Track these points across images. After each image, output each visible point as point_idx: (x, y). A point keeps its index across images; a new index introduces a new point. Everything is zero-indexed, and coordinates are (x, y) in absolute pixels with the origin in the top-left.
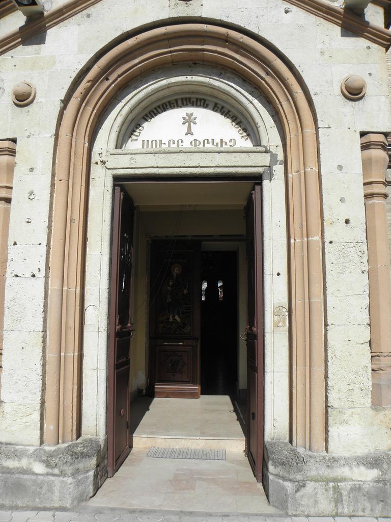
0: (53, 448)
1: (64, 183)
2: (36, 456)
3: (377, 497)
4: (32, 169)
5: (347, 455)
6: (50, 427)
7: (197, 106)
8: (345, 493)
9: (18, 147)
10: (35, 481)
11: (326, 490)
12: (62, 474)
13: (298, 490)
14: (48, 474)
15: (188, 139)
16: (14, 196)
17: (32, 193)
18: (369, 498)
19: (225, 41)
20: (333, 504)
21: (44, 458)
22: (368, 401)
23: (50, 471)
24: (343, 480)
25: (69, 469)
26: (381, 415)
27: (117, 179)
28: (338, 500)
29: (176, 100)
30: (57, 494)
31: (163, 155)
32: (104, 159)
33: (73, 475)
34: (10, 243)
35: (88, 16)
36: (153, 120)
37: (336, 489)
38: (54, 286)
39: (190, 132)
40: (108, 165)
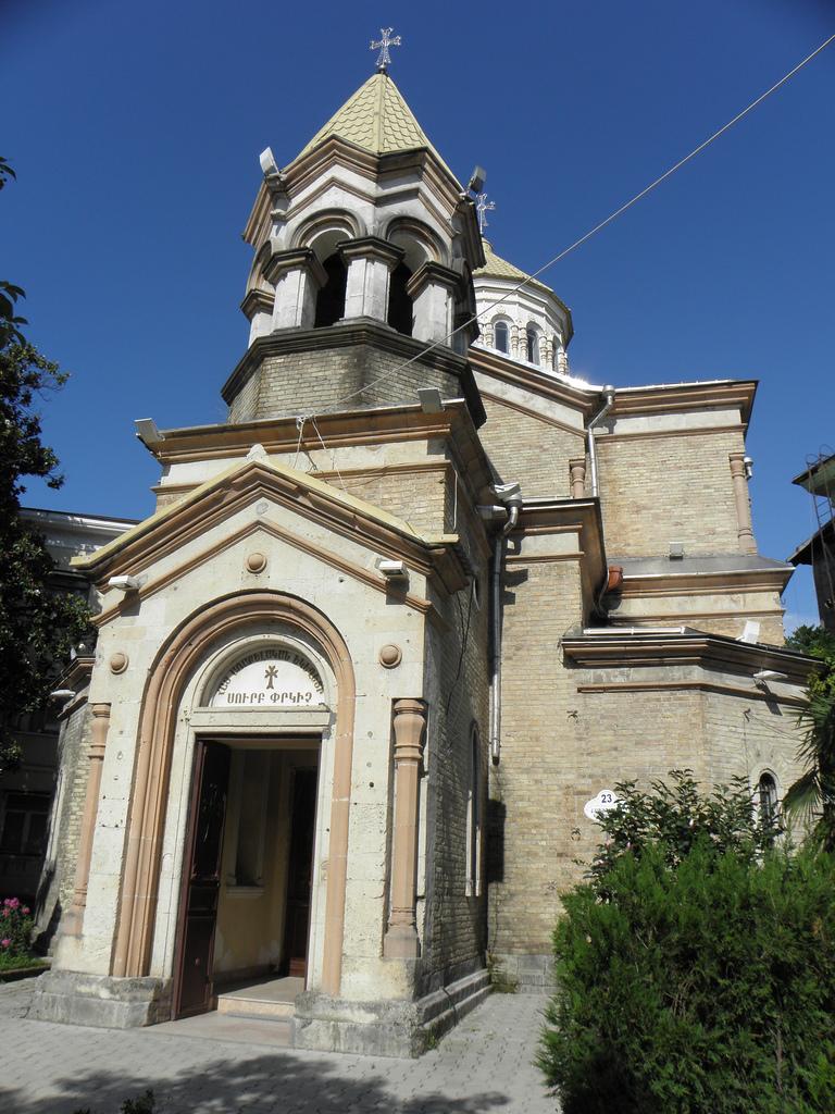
0: (119, 979)
1: (147, 744)
2: (104, 984)
3: (369, 1037)
4: (121, 732)
5: (353, 1000)
6: (119, 960)
7: (280, 658)
8: (342, 1032)
9: (113, 710)
10: (99, 1004)
11: (328, 1028)
12: (122, 999)
13: (304, 1026)
14: (111, 999)
15: (262, 698)
16: (107, 754)
17: (120, 753)
18: (363, 1039)
19: (289, 608)
20: (332, 1041)
21: (109, 985)
22: (378, 951)
23: (112, 996)
24: (344, 1020)
25: (128, 996)
26: (388, 966)
27: (199, 736)
28: (336, 1038)
29: (261, 653)
30: (115, 1016)
31: (237, 715)
32: (188, 716)
33: (130, 1001)
34: (101, 797)
35: (175, 589)
36: (239, 673)
37: (335, 1028)
38: (133, 835)
39: (270, 686)
40: (191, 723)
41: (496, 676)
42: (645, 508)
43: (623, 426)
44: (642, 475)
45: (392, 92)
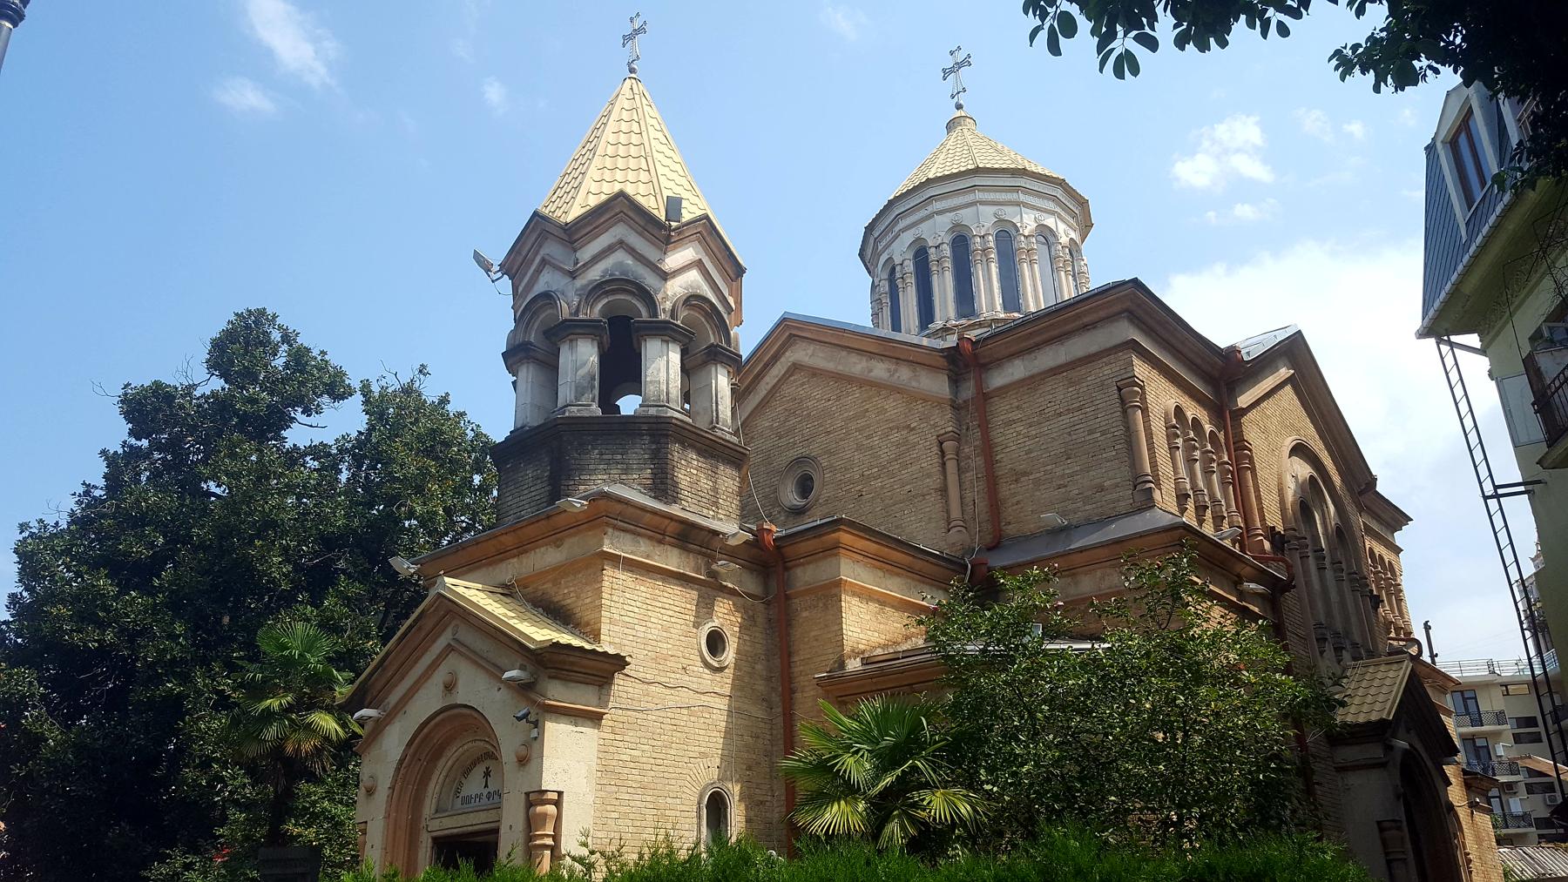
41: (1529, 570)
42: (1025, 474)
43: (998, 379)
44: (1019, 433)
45: (642, 189)
